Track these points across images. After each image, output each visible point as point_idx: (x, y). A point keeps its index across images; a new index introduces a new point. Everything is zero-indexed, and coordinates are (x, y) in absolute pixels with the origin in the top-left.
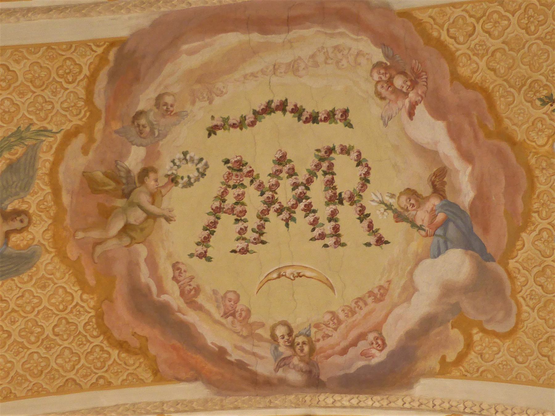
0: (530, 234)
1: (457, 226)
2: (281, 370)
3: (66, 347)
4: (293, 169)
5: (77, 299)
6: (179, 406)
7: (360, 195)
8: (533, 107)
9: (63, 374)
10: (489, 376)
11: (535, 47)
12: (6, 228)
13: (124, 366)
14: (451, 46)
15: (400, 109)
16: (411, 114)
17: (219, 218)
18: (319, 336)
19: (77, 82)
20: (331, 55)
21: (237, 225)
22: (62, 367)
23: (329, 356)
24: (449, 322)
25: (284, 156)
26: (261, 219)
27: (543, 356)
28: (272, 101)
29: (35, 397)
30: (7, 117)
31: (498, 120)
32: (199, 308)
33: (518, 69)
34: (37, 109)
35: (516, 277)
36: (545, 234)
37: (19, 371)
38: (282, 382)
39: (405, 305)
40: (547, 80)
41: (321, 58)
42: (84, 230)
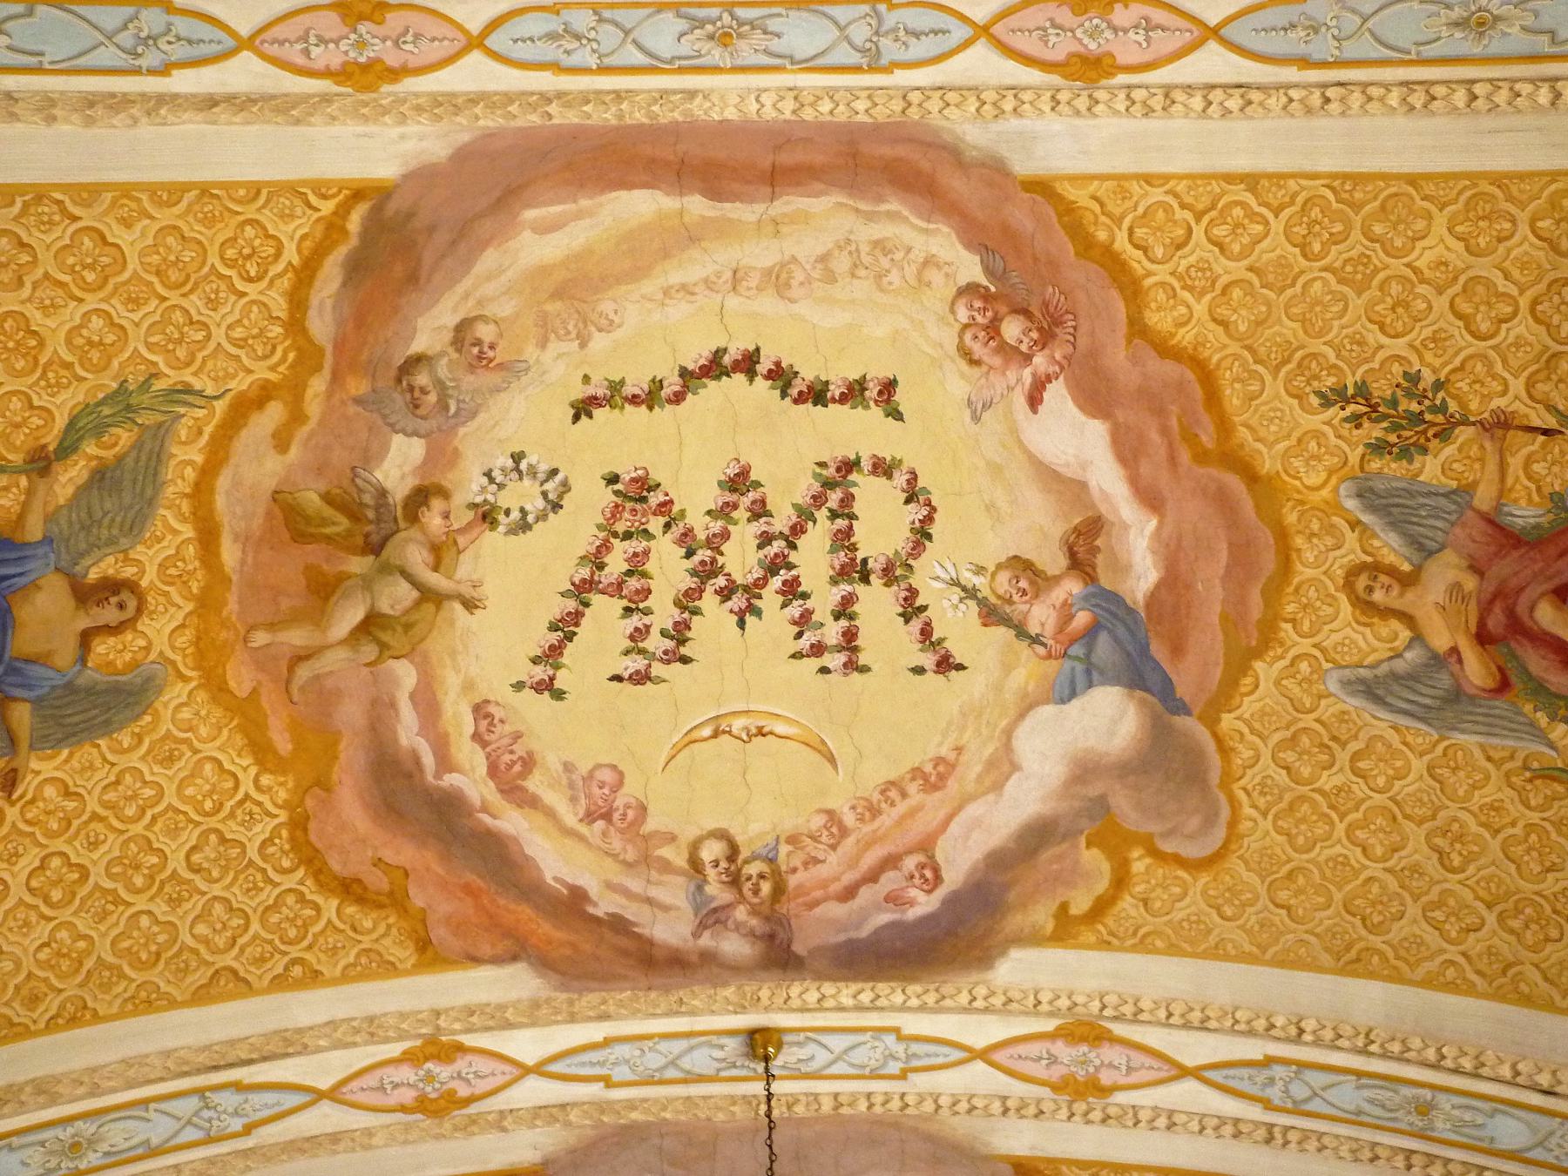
0: (1271, 664)
1: (1116, 640)
2: (707, 934)
3: (215, 898)
4: (763, 502)
5: (247, 786)
6: (474, 1019)
7: (910, 567)
8: (1303, 409)
9: (209, 958)
10: (1159, 943)
11: (1317, 285)
12: (84, 623)
13: (352, 934)
14: (1135, 265)
15: (1010, 389)
16: (1034, 401)
17: (587, 605)
18: (797, 861)
19: (267, 280)
20: (866, 259)
21: (628, 621)
22: (206, 941)
23: (817, 903)
24: (1081, 832)
25: (744, 473)
26: (684, 608)
27: (1277, 906)
28: (725, 350)
29: (144, 1013)
30: (95, 355)
31: (1224, 426)
32: (530, 802)
33: (1276, 328)
34: (170, 340)
35: (1233, 749)
36: (1304, 666)
37: (103, 955)
38: (708, 958)
39: (991, 797)
40: (1338, 356)
41: (842, 264)
42: (271, 626)
